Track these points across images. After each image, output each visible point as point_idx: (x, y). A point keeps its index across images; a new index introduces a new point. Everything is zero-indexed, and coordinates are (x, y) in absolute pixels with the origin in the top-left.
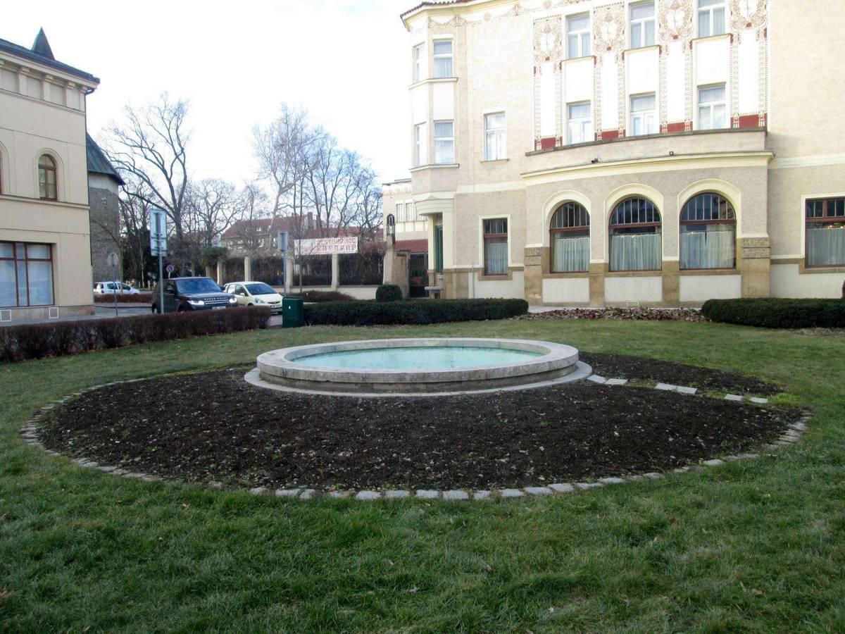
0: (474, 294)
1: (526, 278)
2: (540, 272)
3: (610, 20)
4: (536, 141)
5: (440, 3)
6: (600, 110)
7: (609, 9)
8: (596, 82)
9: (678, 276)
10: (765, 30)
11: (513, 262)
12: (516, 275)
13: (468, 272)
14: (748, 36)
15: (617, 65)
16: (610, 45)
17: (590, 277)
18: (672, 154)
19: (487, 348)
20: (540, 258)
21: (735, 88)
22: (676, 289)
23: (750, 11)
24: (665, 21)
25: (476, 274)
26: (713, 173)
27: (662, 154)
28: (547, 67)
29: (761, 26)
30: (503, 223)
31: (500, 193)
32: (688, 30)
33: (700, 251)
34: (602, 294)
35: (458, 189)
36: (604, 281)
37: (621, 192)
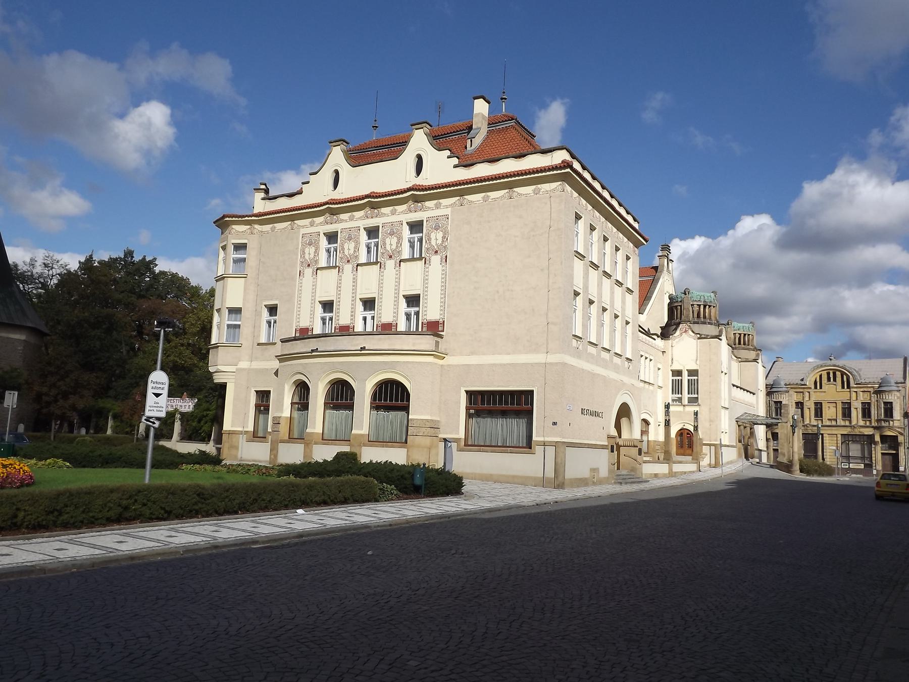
8: (425, 280)
14: (436, 259)
16: (349, 259)
19: (507, 509)
26: (392, 366)
28: (308, 272)
35: (238, 365)
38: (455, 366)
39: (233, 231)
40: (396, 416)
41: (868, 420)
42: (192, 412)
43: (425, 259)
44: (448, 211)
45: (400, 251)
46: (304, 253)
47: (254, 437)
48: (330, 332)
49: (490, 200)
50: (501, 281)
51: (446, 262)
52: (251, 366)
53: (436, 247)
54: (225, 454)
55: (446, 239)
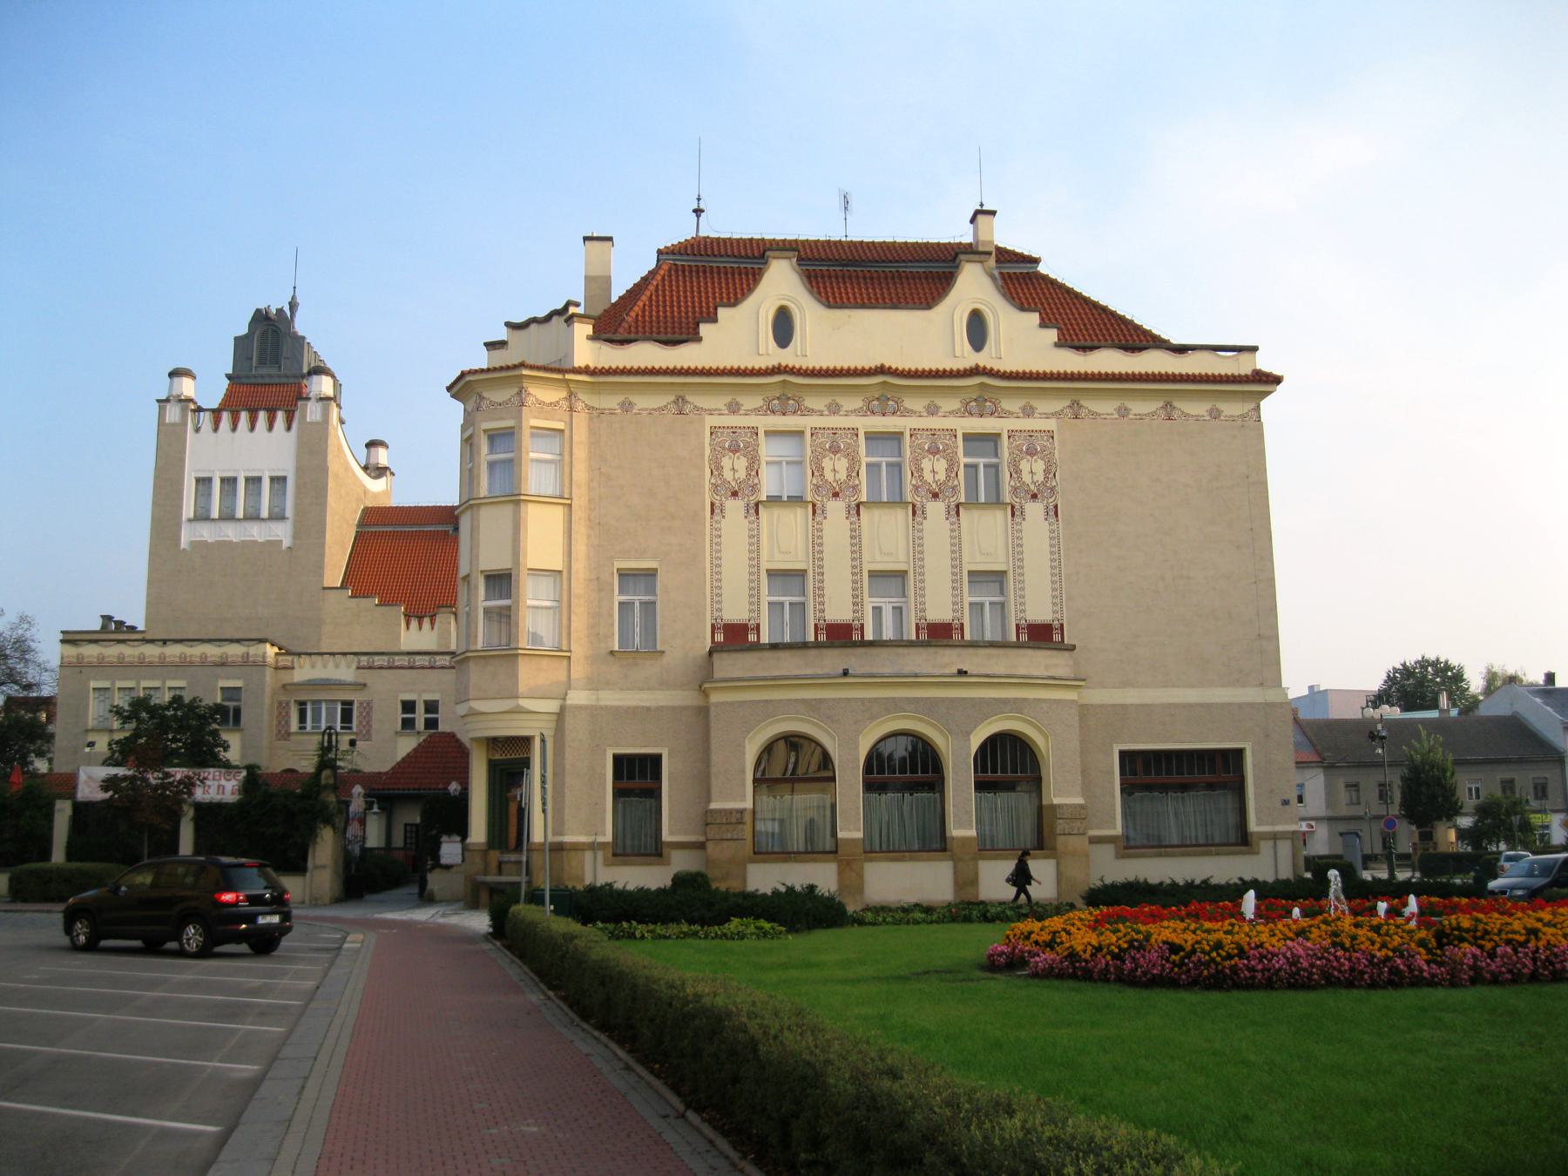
3: (737, 451)
7: (835, 434)
9: (975, 859)
10: (1056, 507)
11: (671, 833)
12: (1265, 847)
14: (1034, 510)
15: (848, 521)
17: (840, 862)
18: (962, 673)
22: (974, 882)
23: (937, 477)
24: (719, 468)
25: (600, 855)
26: (1017, 706)
27: (947, 671)
28: (735, 508)
29: (852, 499)
30: (651, 765)
33: (1206, 826)
36: (862, 868)
37: (1029, 727)
39: (530, 401)
40: (1020, 800)
42: (238, 806)
43: (1013, 507)
44: (1051, 424)
47: (755, 853)
49: (1131, 416)
50: (1166, 561)
51: (1057, 516)
52: (598, 699)
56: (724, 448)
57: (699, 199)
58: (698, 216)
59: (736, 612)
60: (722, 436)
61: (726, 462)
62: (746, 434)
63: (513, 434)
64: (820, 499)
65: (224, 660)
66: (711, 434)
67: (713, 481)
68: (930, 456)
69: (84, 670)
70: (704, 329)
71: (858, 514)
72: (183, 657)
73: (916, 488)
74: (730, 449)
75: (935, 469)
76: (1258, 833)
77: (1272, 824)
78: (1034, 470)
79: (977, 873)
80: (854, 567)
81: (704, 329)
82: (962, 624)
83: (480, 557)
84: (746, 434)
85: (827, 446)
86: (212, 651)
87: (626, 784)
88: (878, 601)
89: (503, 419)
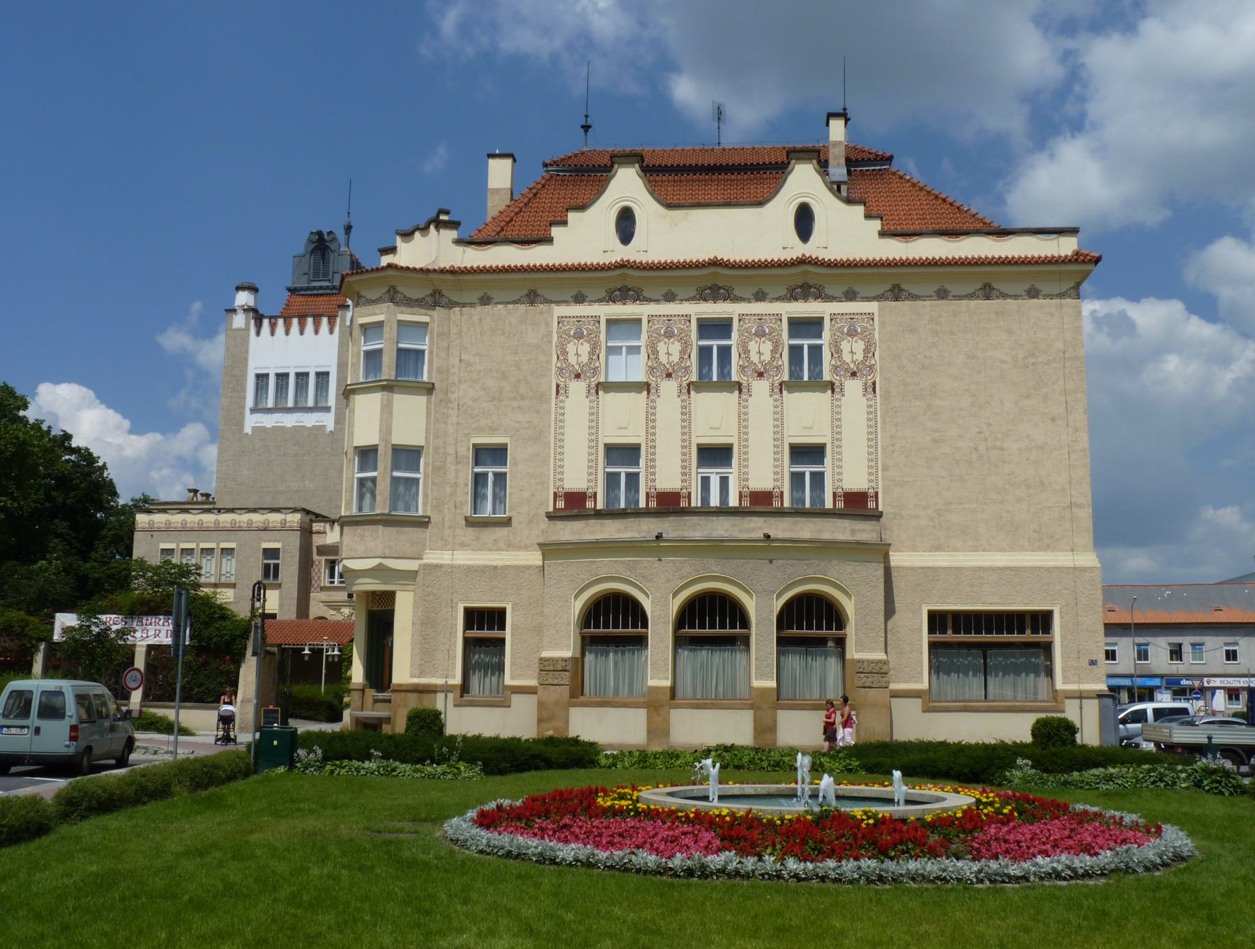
0: (1082, 741)
1: (541, 705)
2: (567, 695)
3: (671, 337)
4: (555, 494)
5: (372, 270)
6: (654, 460)
10: (874, 384)
13: (435, 692)
14: (853, 388)
16: (670, 370)
20: (567, 673)
21: (838, 453)
22: (772, 728)
23: (671, 359)
25: (450, 696)
28: (578, 389)
31: (495, 568)
32: (778, 368)
34: (667, 733)
35: (424, 556)
38: (908, 568)
41: (699, 699)
45: (597, 367)
46: (747, 351)
48: (354, 511)
50: (981, 432)
53: (760, 366)
54: (678, 706)
55: (871, 353)
56: (569, 336)
57: (587, 116)
58: (586, 131)
59: (576, 481)
60: (568, 325)
61: (571, 348)
62: (863, 319)
63: (383, 326)
64: (654, 379)
65: (266, 525)
66: (559, 323)
67: (559, 365)
68: (849, 338)
69: (154, 533)
70: (556, 231)
71: (597, 394)
72: (233, 522)
73: (743, 368)
74: (756, 334)
75: (761, 351)
76: (1064, 691)
77: (1079, 683)
78: (853, 350)
79: (775, 722)
80: (683, 441)
81: (556, 231)
82: (782, 492)
83: (355, 435)
84: (589, 322)
85: (662, 332)
86: (257, 518)
87: (938, 637)
88: (705, 471)
89: (374, 314)
